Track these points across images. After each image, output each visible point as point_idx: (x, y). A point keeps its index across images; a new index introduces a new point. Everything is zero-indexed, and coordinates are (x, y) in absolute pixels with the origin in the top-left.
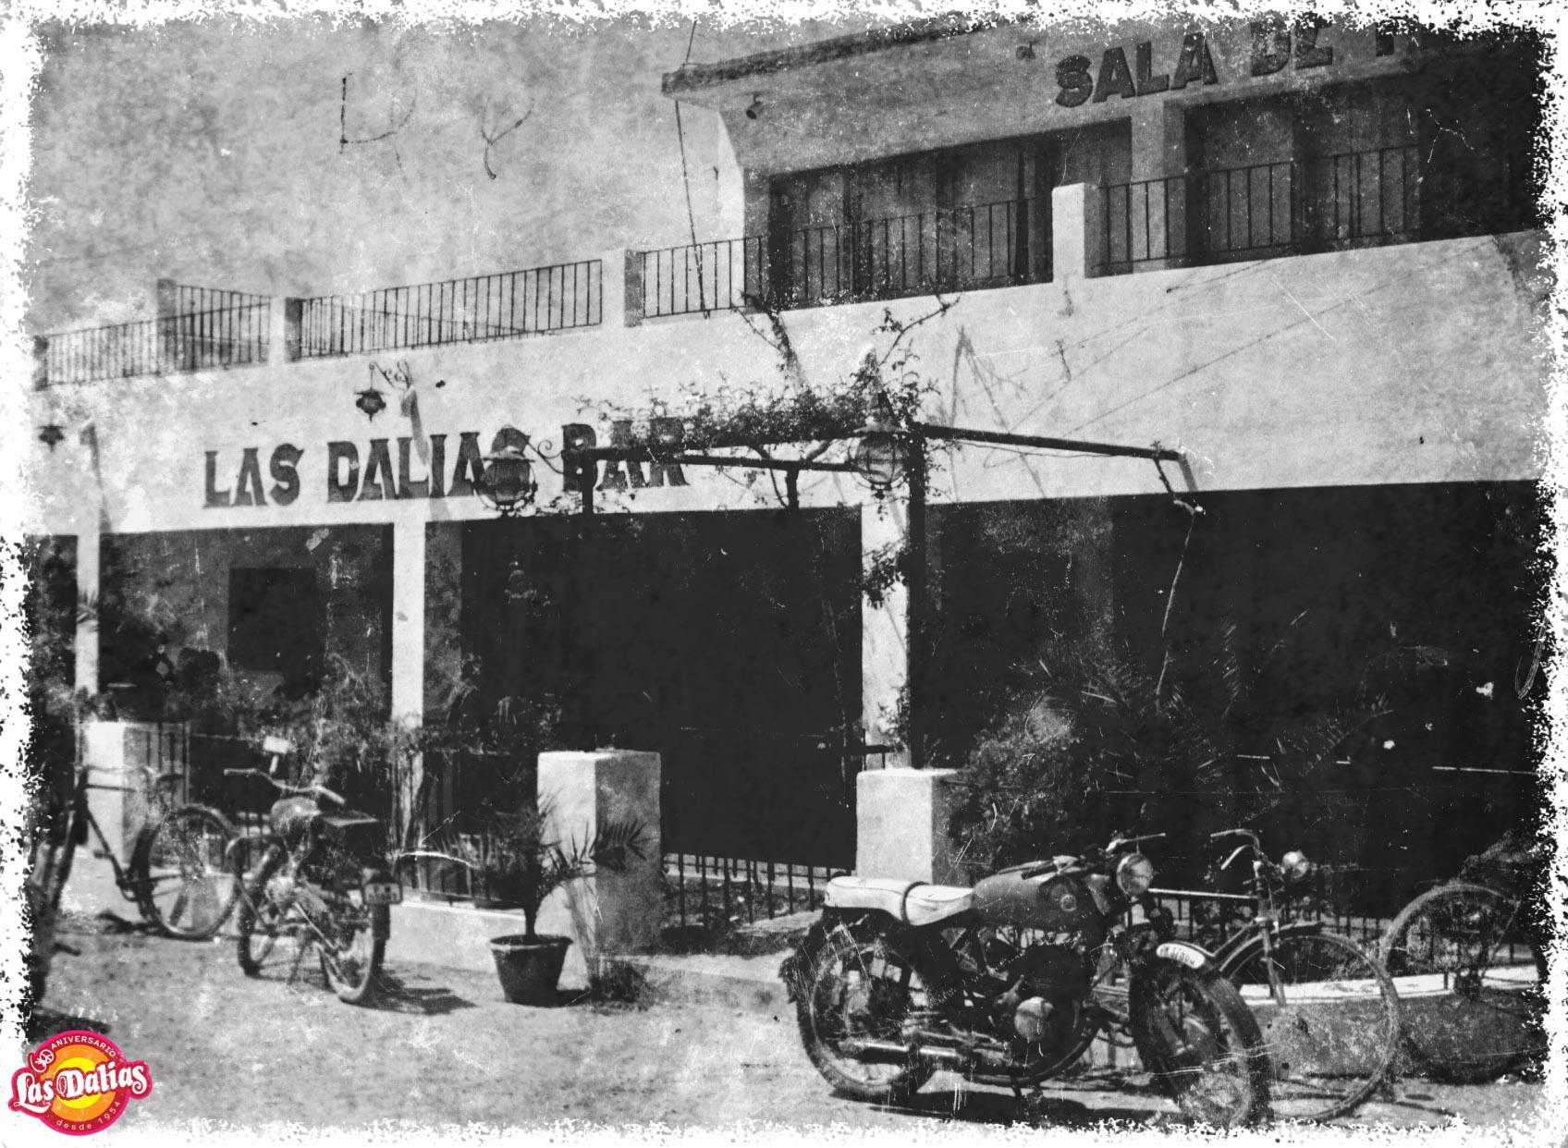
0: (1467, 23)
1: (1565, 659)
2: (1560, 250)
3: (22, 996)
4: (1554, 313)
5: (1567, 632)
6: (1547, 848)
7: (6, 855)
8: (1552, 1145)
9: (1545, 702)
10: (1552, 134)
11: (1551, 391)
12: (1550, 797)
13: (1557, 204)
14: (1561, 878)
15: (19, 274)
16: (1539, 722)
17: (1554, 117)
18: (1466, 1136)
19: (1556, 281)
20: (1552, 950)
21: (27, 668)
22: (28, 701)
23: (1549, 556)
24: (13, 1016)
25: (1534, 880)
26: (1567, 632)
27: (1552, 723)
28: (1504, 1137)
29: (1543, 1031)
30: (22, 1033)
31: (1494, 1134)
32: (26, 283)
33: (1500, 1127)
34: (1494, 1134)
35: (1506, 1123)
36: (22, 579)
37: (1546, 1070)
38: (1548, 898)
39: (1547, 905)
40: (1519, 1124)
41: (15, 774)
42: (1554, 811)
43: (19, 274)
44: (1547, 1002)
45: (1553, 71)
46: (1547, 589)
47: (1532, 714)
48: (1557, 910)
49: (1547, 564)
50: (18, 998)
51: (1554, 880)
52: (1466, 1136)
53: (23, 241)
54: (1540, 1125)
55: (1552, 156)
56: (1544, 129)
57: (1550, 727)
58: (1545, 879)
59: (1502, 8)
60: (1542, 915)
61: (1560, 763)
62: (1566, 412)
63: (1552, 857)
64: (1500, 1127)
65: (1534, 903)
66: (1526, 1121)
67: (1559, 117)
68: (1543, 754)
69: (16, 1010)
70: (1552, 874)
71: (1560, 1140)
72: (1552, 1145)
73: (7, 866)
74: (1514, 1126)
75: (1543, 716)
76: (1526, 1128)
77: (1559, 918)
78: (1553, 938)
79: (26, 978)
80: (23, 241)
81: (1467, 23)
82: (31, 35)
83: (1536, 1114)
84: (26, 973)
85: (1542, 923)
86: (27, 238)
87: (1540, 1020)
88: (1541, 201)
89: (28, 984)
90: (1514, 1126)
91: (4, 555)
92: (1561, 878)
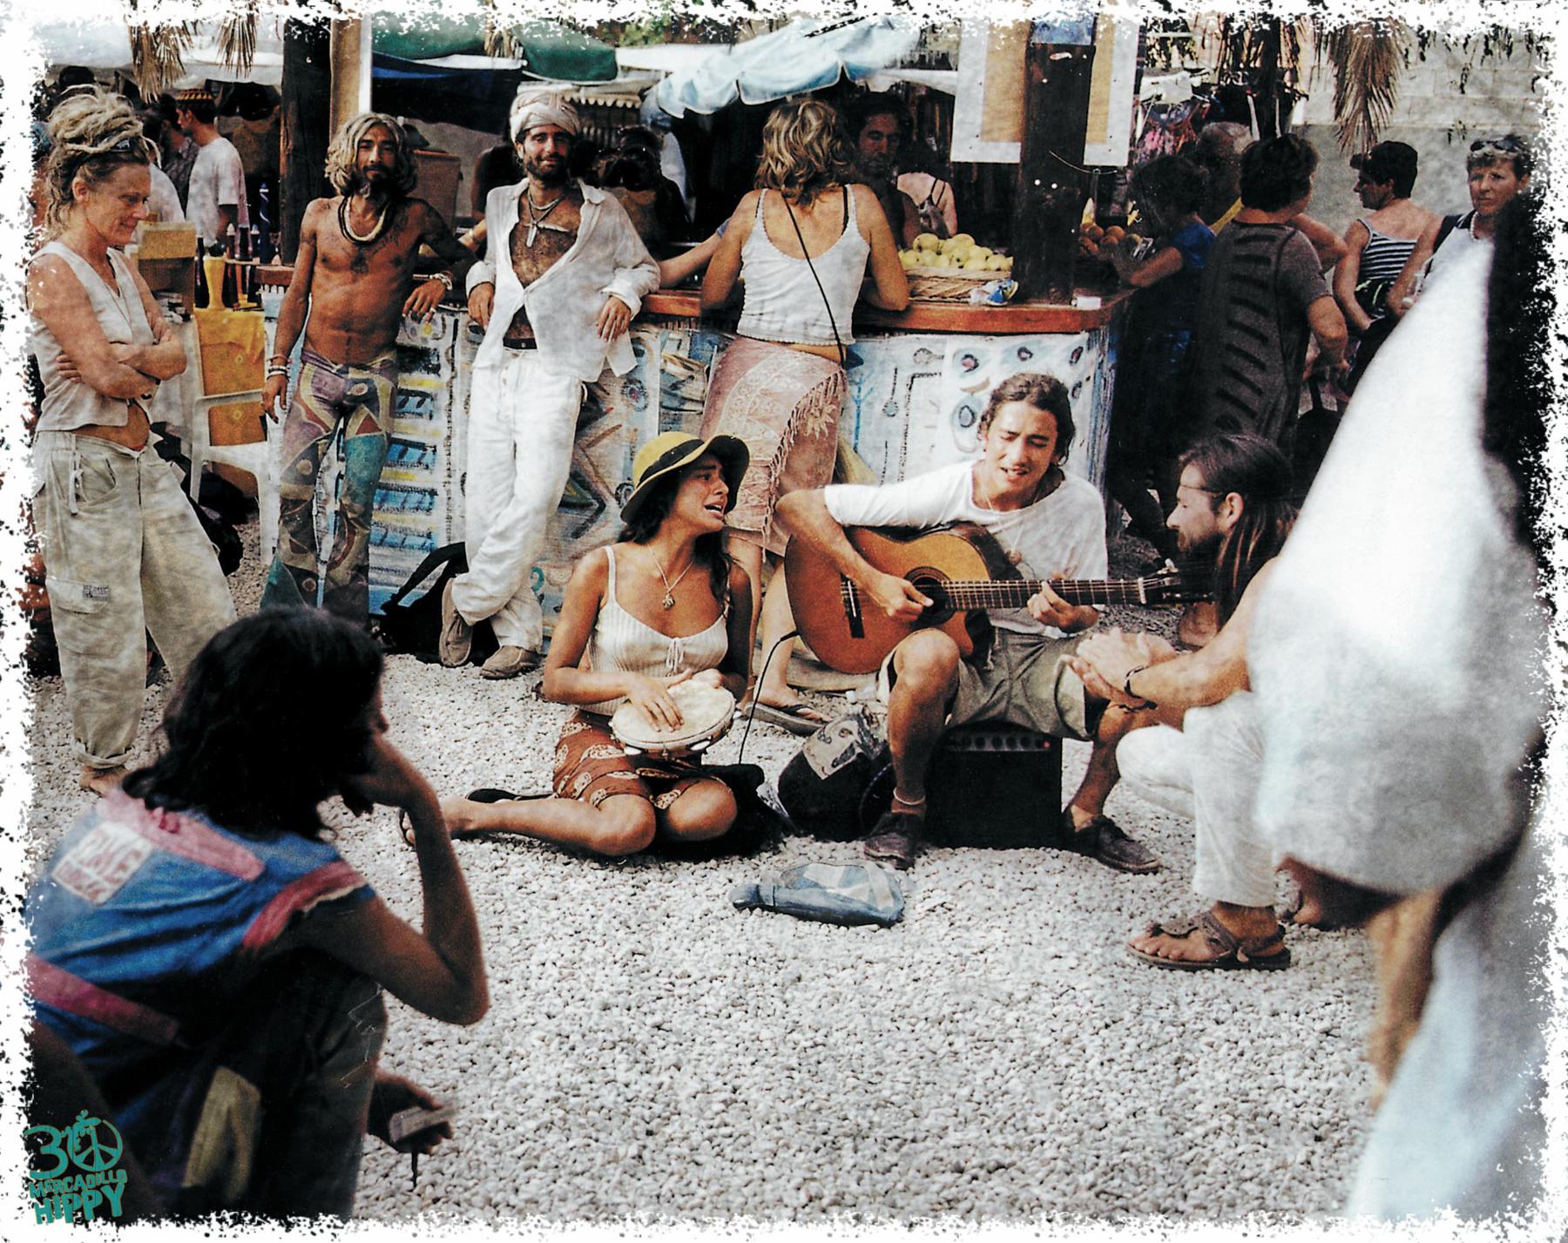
0: (1458, 25)
1: (1564, 714)
2: (1560, 272)
3: (24, 1078)
4: (1553, 647)
5: (1567, 684)
6: (1545, 304)
7: (7, 619)
8: (1551, 1239)
9: (1542, 1151)
10: (1551, 146)
11: (1550, 424)
12: (1548, 249)
13: (1555, 528)
14: (1560, 337)
15: (21, 910)
16: (1537, 474)
17: (1553, 127)
18: (1458, 1230)
19: (1555, 611)
20: (1551, 415)
21: (29, 1030)
22: (31, 1065)
23: (1547, 295)
24: (14, 1100)
25: (1532, 952)
26: (1567, 684)
27: (1551, 476)
28: (1498, 1231)
29: (1541, 1116)
30: (24, 1119)
31: (1488, 1228)
32: (28, 614)
33: (1494, 1220)
34: (1488, 1228)
35: (1501, 1216)
36: (24, 934)
37: (1544, 1158)
38: (1546, 358)
39: (1546, 367)
40: (1515, 1217)
41: (16, 224)
42: (1553, 265)
43: (21, 910)
44: (1546, 1084)
45: (1552, 77)
46: (1545, 331)
47: (1528, 466)
48: (1556, 372)
49: (1545, 918)
50: (19, 1080)
51: (1552, 339)
52: (1458, 1230)
53: (25, 568)
54: (1538, 1218)
55: (1551, 169)
56: (1542, 140)
57: (1549, 481)
58: (1543, 337)
59: (1497, 8)
60: (1540, 377)
61: (1559, 213)
62: (1567, 1060)
63: (1551, 314)
64: (1494, 1220)
65: (1531, 364)
66: (1522, 1214)
67: (1558, 126)
68: (1541, 510)
69: (18, 1094)
70: (1551, 333)
71: (1559, 1235)
72: (1551, 1239)
73: (8, 937)
74: (1509, 1220)
75: (1541, 468)
76: (1523, 1222)
77: (1558, 380)
78: (1552, 401)
79: (28, 1059)
80: (25, 568)
81: (1458, 25)
82: (33, 38)
83: (1534, 1205)
84: (28, 1053)
85: (1540, 386)
86: (29, 564)
87: (1539, 1104)
88: (1538, 218)
89: (31, 1065)
90: (1509, 1220)
91: (5, 601)
92: (1560, 337)
